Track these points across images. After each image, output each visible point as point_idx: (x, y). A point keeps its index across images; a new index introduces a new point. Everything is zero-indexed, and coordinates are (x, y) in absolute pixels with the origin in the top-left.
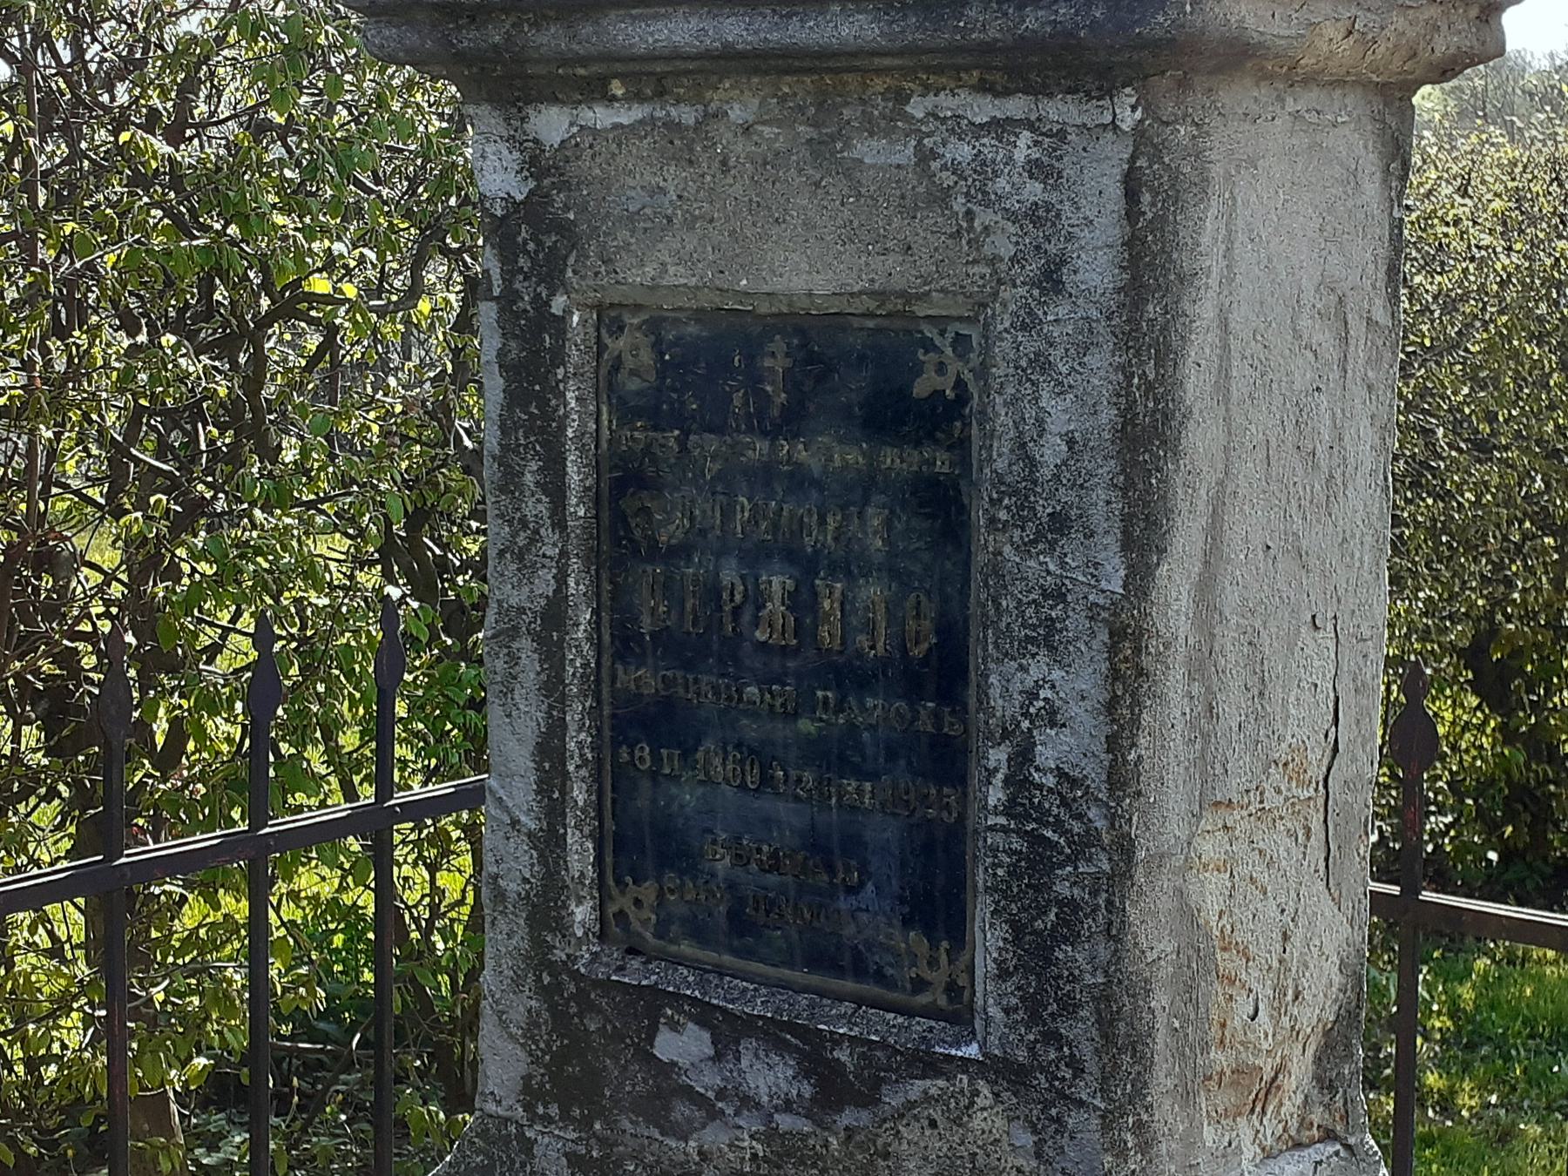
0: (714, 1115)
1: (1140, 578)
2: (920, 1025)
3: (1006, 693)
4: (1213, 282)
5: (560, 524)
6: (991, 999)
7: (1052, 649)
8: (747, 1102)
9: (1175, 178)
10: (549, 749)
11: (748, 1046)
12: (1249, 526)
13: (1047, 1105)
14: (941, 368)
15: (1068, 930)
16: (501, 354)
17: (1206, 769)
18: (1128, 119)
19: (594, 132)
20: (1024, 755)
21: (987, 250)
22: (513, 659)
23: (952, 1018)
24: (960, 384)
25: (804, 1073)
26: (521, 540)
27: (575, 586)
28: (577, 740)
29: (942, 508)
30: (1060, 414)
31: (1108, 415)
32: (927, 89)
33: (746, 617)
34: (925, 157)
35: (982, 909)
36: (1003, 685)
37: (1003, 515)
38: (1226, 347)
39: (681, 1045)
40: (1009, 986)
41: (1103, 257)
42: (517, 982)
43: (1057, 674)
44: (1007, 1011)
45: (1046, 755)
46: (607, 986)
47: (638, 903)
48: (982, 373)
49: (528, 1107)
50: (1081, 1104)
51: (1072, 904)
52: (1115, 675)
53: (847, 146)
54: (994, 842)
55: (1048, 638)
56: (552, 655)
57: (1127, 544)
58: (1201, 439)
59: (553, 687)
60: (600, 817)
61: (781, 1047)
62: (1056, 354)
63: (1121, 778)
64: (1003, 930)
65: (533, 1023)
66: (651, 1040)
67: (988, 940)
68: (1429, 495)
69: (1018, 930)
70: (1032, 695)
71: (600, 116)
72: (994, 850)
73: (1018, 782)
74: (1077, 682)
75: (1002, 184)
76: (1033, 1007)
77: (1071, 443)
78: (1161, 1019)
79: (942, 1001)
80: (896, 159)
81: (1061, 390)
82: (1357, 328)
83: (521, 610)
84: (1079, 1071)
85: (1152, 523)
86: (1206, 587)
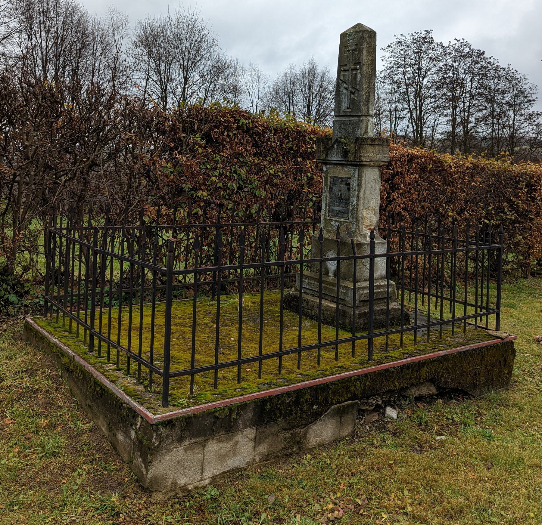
1: (359, 193)
10: (326, 205)
12: (367, 192)
17: (364, 205)
28: (327, 204)
29: (349, 189)
36: (351, 199)
39: (333, 223)
54: (351, 209)
55: (354, 197)
56: (326, 199)
58: (363, 186)
63: (357, 205)
67: (350, 214)
68: (154, 145)
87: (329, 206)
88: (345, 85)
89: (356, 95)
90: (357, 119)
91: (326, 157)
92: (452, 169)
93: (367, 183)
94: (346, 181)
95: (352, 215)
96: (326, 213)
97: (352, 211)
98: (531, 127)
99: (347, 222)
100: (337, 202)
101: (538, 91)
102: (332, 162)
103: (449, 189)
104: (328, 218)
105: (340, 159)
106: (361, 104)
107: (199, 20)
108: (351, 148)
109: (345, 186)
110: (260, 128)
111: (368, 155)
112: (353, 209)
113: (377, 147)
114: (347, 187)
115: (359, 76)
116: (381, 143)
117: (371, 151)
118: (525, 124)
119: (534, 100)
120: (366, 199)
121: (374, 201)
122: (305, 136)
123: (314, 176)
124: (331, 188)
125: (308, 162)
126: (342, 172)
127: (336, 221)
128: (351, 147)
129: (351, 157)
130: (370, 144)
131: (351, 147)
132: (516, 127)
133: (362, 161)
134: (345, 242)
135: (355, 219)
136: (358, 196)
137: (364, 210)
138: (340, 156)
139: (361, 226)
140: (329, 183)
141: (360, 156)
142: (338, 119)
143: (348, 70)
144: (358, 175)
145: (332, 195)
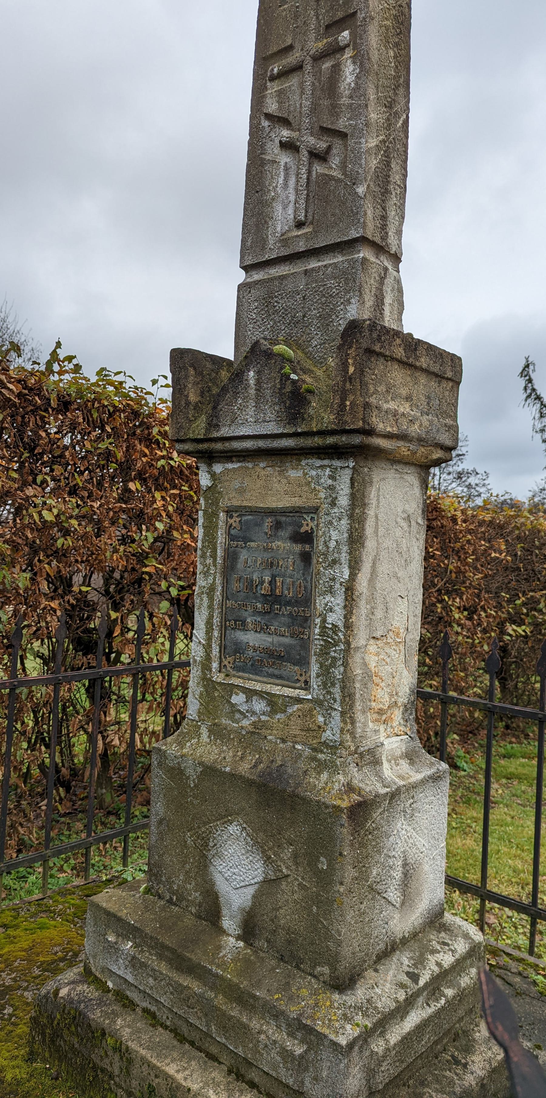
0: (245, 717)
2: (297, 691)
3: (320, 605)
4: (374, 506)
5: (215, 565)
6: (314, 683)
7: (331, 593)
8: (254, 713)
9: (363, 480)
10: (209, 624)
11: (255, 698)
12: (383, 568)
13: (327, 710)
14: (307, 525)
15: (333, 665)
16: (203, 524)
18: (352, 465)
19: (228, 470)
20: (324, 621)
21: (319, 497)
22: (202, 600)
23: (305, 689)
24: (312, 528)
25: (268, 705)
26: (205, 569)
27: (218, 581)
29: (306, 558)
30: (334, 535)
31: (346, 535)
32: (306, 458)
33: (259, 588)
34: (305, 474)
35: (313, 659)
36: (320, 603)
37: (321, 560)
38: (377, 523)
39: (238, 699)
40: (319, 680)
41: (345, 498)
42: (198, 683)
43: (333, 599)
44: (318, 686)
45: (329, 620)
46: (220, 684)
47: (229, 662)
48: (317, 526)
49: (199, 717)
50: (335, 709)
51: (334, 658)
52: (346, 599)
53: (287, 472)
54: (317, 644)
55: (331, 591)
56: (211, 599)
57: (350, 567)
58: (370, 544)
59: (211, 607)
60: (221, 640)
61: (262, 697)
62: (334, 521)
63: (348, 626)
64: (318, 665)
65: (201, 694)
66: (230, 698)
67: (314, 668)
69: (321, 665)
70: (326, 605)
71: (230, 466)
72: (316, 645)
73: (323, 627)
74: (338, 601)
75: (322, 480)
76: (325, 684)
77: (337, 542)
78: (357, 690)
79: (303, 685)
80: (298, 475)
81: (335, 529)
82: (413, 523)
83: (204, 587)
84: (335, 701)
85: (356, 562)
86: (372, 581)
87: (224, 628)
88: (286, 133)
89: (335, 161)
90: (340, 258)
91: (213, 425)
92: (457, 524)
93: (381, 531)
94: (298, 528)
95: (325, 672)
96: (208, 658)
97: (324, 652)
98: (461, 489)
99: (299, 700)
100: (256, 612)
101: (467, 443)
102: (236, 445)
103: (453, 564)
104: (218, 678)
105: (272, 428)
106: (361, 190)
107: (10, 319)
108: (318, 378)
109: (288, 545)
110: (11, 386)
111: (392, 405)
112: (327, 646)
113: (423, 379)
114: (297, 548)
115: (349, 73)
116: (436, 368)
117: (404, 392)
118: (454, 485)
119: (464, 455)
120: (379, 600)
121: (403, 606)
122: (149, 427)
123: (176, 534)
124: (231, 558)
125: (158, 495)
126: (276, 488)
127: (250, 693)
128: (316, 379)
129: (321, 415)
130: (400, 362)
131: (316, 379)
132: (443, 488)
133: (370, 432)
134: (294, 795)
135: (337, 691)
136: (350, 589)
137: (372, 648)
138: (270, 415)
139: (359, 717)
140: (221, 537)
141: (367, 406)
142: (257, 276)
143: (299, 68)
144: (353, 497)
145: (235, 586)
